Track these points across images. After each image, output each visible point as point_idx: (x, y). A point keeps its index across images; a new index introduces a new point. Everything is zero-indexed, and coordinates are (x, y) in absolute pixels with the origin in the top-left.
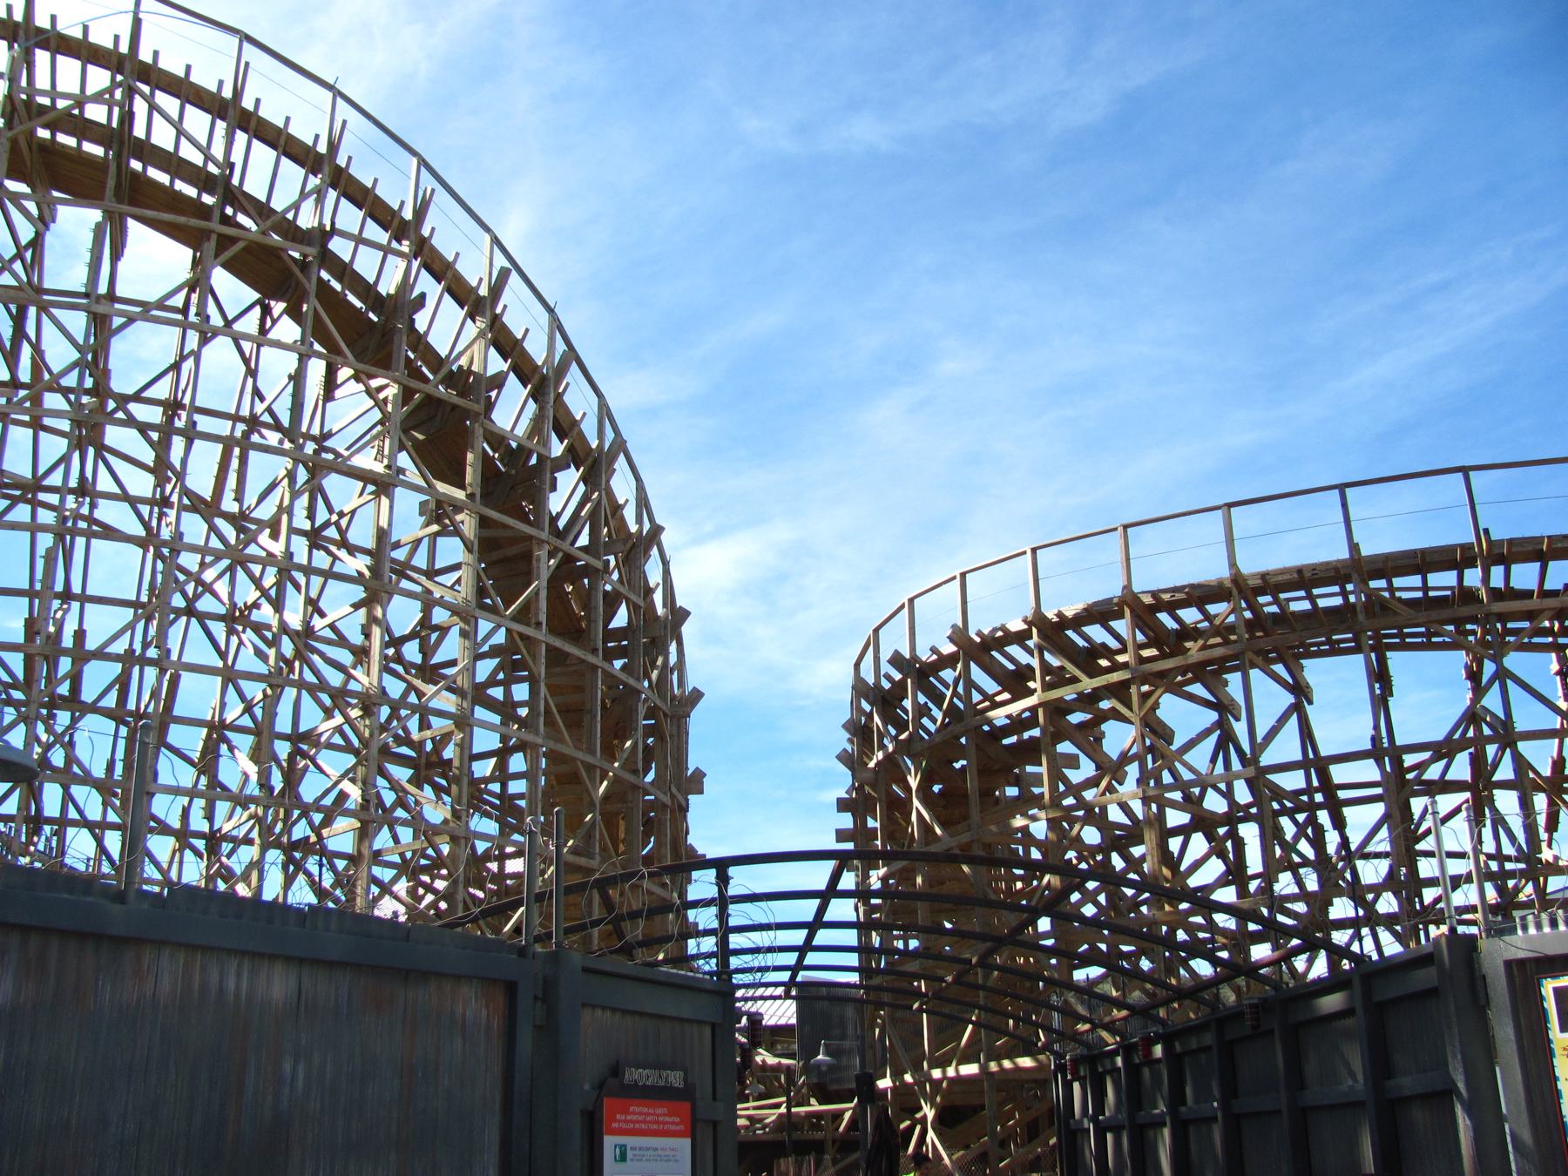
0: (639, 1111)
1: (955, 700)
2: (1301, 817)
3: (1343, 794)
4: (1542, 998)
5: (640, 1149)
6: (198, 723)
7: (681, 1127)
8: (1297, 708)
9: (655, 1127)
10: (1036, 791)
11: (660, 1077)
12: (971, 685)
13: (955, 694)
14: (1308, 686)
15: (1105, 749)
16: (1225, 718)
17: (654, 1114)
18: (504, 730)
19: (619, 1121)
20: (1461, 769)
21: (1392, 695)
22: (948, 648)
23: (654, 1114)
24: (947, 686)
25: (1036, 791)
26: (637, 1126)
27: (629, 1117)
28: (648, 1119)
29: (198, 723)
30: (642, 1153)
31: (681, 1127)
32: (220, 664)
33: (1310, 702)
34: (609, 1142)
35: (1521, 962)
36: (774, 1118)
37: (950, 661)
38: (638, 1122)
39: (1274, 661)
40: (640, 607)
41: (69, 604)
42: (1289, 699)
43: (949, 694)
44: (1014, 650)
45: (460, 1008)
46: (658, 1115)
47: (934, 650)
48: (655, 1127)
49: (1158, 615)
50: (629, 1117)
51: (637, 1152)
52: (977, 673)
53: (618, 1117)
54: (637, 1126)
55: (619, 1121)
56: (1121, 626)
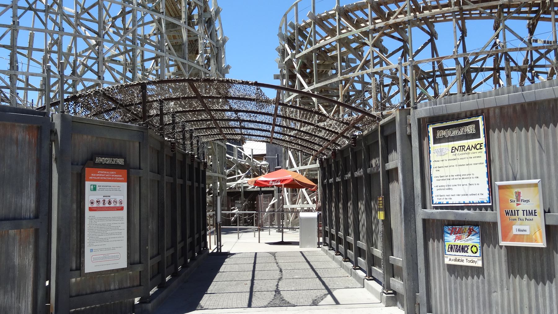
0: (102, 173)
1: (311, 38)
2: (430, 80)
3: (447, 72)
4: (428, 132)
5: (103, 186)
6: (41, 50)
7: (123, 179)
8: (431, 41)
9: (110, 178)
11: (113, 160)
12: (316, 32)
13: (311, 36)
14: (436, 33)
15: (28, 11)
16: (405, 44)
17: (110, 174)
18: (156, 52)
19: (93, 176)
20: (490, 63)
21: (466, 36)
22: (309, 21)
23: (110, 174)
24: (308, 33)
26: (101, 178)
27: (97, 175)
28: (107, 176)
29: (41, 50)
30: (104, 188)
31: (123, 179)
32: (44, 28)
33: (436, 39)
34: (88, 184)
35: (424, 119)
36: (235, 184)
37: (309, 25)
38: (101, 177)
39: (423, 24)
40: (202, 7)
41: (499, 73)
42: (429, 37)
43: (308, 36)
44: (331, 20)
45: (15, 135)
46: (111, 174)
47: (304, 21)
48: (110, 178)
49: (381, 7)
50: (97, 175)
51: (102, 187)
52: (318, 28)
53: (92, 175)
54: (101, 178)
55: (93, 176)
56: (368, 11)
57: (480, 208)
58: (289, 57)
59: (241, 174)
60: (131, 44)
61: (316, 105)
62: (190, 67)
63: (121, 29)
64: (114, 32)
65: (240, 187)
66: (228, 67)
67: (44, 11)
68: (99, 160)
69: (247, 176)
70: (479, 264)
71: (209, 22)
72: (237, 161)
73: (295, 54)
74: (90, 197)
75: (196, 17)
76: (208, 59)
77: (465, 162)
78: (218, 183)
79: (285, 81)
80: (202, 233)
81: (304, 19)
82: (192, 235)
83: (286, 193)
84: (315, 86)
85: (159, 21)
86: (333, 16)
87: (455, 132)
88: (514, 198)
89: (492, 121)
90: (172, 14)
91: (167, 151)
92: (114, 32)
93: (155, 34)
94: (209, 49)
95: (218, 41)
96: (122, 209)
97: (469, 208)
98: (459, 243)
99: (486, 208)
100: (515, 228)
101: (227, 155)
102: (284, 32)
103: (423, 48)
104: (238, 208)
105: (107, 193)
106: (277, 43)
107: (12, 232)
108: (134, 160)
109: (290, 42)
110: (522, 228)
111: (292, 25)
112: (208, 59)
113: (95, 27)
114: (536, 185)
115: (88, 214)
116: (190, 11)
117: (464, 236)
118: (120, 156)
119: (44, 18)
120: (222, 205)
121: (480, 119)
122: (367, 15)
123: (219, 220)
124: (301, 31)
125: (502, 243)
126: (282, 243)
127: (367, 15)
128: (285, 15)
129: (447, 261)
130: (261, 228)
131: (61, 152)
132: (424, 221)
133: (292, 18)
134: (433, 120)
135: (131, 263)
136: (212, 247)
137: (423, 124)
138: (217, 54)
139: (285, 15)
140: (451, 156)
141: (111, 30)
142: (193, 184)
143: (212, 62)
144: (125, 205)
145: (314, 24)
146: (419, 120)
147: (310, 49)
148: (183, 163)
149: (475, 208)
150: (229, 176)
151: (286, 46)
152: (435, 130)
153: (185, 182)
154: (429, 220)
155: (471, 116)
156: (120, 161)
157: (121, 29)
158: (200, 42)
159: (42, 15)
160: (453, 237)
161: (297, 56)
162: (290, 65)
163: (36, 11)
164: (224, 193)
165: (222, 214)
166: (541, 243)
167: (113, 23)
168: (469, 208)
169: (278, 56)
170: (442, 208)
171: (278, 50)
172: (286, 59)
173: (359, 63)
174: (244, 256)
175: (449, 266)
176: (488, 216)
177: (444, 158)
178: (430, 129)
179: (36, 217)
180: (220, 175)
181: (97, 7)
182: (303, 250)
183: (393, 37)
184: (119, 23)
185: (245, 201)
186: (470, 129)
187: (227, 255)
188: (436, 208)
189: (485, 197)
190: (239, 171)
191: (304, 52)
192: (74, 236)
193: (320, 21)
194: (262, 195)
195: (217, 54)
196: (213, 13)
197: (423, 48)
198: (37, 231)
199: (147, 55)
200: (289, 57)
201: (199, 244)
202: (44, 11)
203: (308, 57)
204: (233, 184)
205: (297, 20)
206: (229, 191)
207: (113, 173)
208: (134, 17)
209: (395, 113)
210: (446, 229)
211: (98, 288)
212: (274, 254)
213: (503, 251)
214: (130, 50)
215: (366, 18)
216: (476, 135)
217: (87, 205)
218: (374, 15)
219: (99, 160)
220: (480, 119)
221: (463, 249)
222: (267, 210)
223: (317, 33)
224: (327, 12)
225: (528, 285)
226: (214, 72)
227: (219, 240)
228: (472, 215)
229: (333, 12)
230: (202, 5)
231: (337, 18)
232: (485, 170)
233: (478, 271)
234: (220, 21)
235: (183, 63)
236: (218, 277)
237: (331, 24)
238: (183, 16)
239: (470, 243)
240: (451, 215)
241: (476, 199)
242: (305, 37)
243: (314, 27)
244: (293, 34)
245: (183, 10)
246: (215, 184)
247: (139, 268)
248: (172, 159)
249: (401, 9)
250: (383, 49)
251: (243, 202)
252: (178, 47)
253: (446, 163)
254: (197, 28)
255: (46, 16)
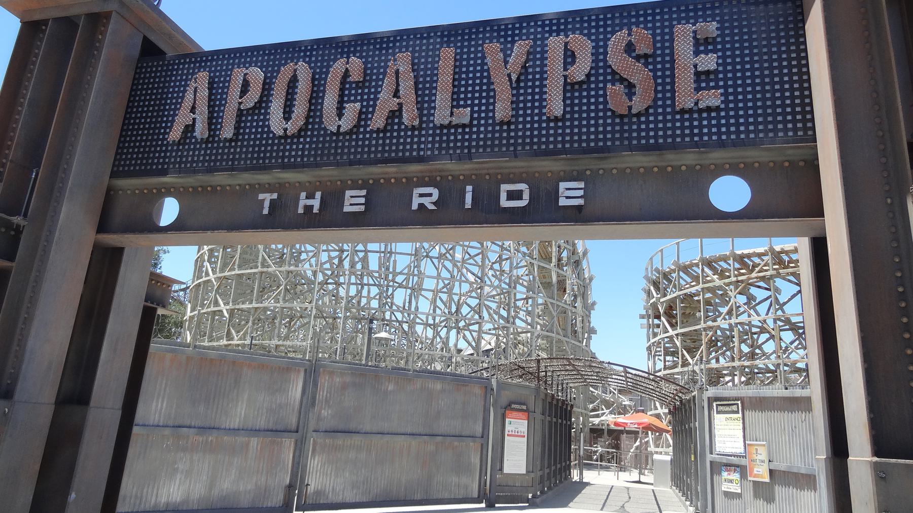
0: (515, 414)
10: (709, 62)
12: (680, 277)
13: (675, 280)
22: (673, 267)
25: (709, 62)
34: (507, 420)
37: (674, 271)
52: (682, 274)
56: (731, 262)
57: (740, 456)
58: (654, 300)
59: (605, 411)
60: (507, 287)
61: (680, 350)
62: (558, 306)
63: (498, 271)
64: (493, 275)
65: (603, 425)
66: (594, 303)
67: (437, 258)
68: (513, 406)
69: (611, 413)
70: (739, 491)
71: (577, 263)
72: (601, 396)
73: (660, 298)
74: (508, 428)
75: (565, 259)
76: (575, 296)
77: (732, 427)
78: (581, 418)
79: (651, 320)
80: (568, 463)
81: (668, 265)
82: (555, 464)
83: (650, 437)
84: (679, 331)
85: (532, 264)
86: (697, 265)
87: (727, 409)
88: (755, 452)
89: (746, 405)
90: (544, 257)
91: (549, 400)
92: (493, 275)
93: (527, 275)
94: (576, 288)
95: (585, 278)
96: (524, 436)
97: (734, 456)
98: (730, 477)
99: (743, 456)
100: (755, 469)
101: (591, 389)
102: (650, 275)
103: (790, 300)
104: (601, 446)
105: (516, 426)
106: (644, 284)
107: (471, 444)
108: (532, 408)
109: (656, 284)
110: (759, 470)
111: (657, 270)
112: (575, 296)
113: (476, 270)
114: (764, 445)
115: (507, 438)
116: (560, 253)
117: (732, 473)
118: (524, 404)
119: (436, 263)
120: (585, 441)
121: (739, 402)
122: (730, 265)
123: (582, 453)
124: (666, 276)
125: (749, 478)
126: (639, 482)
127: (730, 265)
128: (651, 259)
129: (723, 489)
130: (622, 469)
131: (496, 402)
132: (711, 462)
133: (657, 264)
134: (717, 399)
135: (528, 472)
136: (576, 477)
137: (710, 401)
138: (584, 293)
139: (651, 259)
140: (725, 423)
141: (491, 273)
142: (557, 420)
143: (579, 299)
144: (526, 434)
145: (678, 271)
146: (709, 398)
147: (678, 293)
148: (557, 405)
149: (737, 456)
150: (591, 411)
151: (652, 288)
152: (717, 405)
153: (552, 419)
154: (776, 471)
155: (736, 400)
156: (524, 407)
157: (498, 271)
158: (568, 282)
159: (436, 261)
160: (726, 473)
161: (662, 300)
162: (654, 306)
163: (431, 258)
164: (587, 430)
165: (584, 449)
166: (767, 480)
167: (491, 266)
168: (734, 456)
169: (644, 296)
170: (721, 455)
171: (644, 290)
172: (652, 301)
173: (724, 310)
174: (603, 487)
175: (724, 492)
176: (743, 462)
177: (722, 423)
178: (714, 404)
179: (482, 437)
180: (583, 411)
181: (480, 256)
182: (654, 488)
183: (759, 287)
184: (497, 266)
185: (608, 440)
186: (734, 408)
187: (588, 484)
188: (718, 454)
189: (742, 450)
190: (603, 407)
191: (668, 297)
192: (499, 450)
193: (685, 269)
194: (625, 435)
195: (584, 293)
196: (581, 254)
197: (790, 300)
198: (482, 445)
199: (519, 296)
200: (654, 300)
201: (565, 471)
202: (437, 258)
203: (673, 300)
204: (596, 421)
205: (662, 266)
206: (592, 427)
207: (520, 414)
208: (511, 264)
209: (695, 393)
210: (723, 468)
211: (509, 484)
212: (628, 489)
213: (751, 483)
214: (506, 293)
215: (729, 267)
216: (737, 412)
217: (506, 433)
218: (737, 266)
219: (513, 406)
220: (739, 402)
221: (731, 481)
222: (632, 451)
223: (682, 278)
224: (691, 261)
225: (763, 505)
226: (580, 309)
227: (581, 474)
228: (735, 460)
229: (696, 261)
230: (571, 248)
231: (700, 266)
232: (742, 434)
233: (738, 496)
234: (587, 260)
235: (552, 303)
236: (580, 495)
237: (695, 272)
238: (554, 260)
239: (734, 478)
240: (725, 460)
241: (734, 451)
242: (670, 281)
243: (679, 274)
244: (659, 278)
245: (554, 254)
246: (578, 419)
247: (532, 475)
248: (551, 403)
249: (765, 262)
250: (750, 297)
251: (606, 440)
252: (547, 285)
253: (723, 427)
254: (565, 268)
255: (439, 262)
